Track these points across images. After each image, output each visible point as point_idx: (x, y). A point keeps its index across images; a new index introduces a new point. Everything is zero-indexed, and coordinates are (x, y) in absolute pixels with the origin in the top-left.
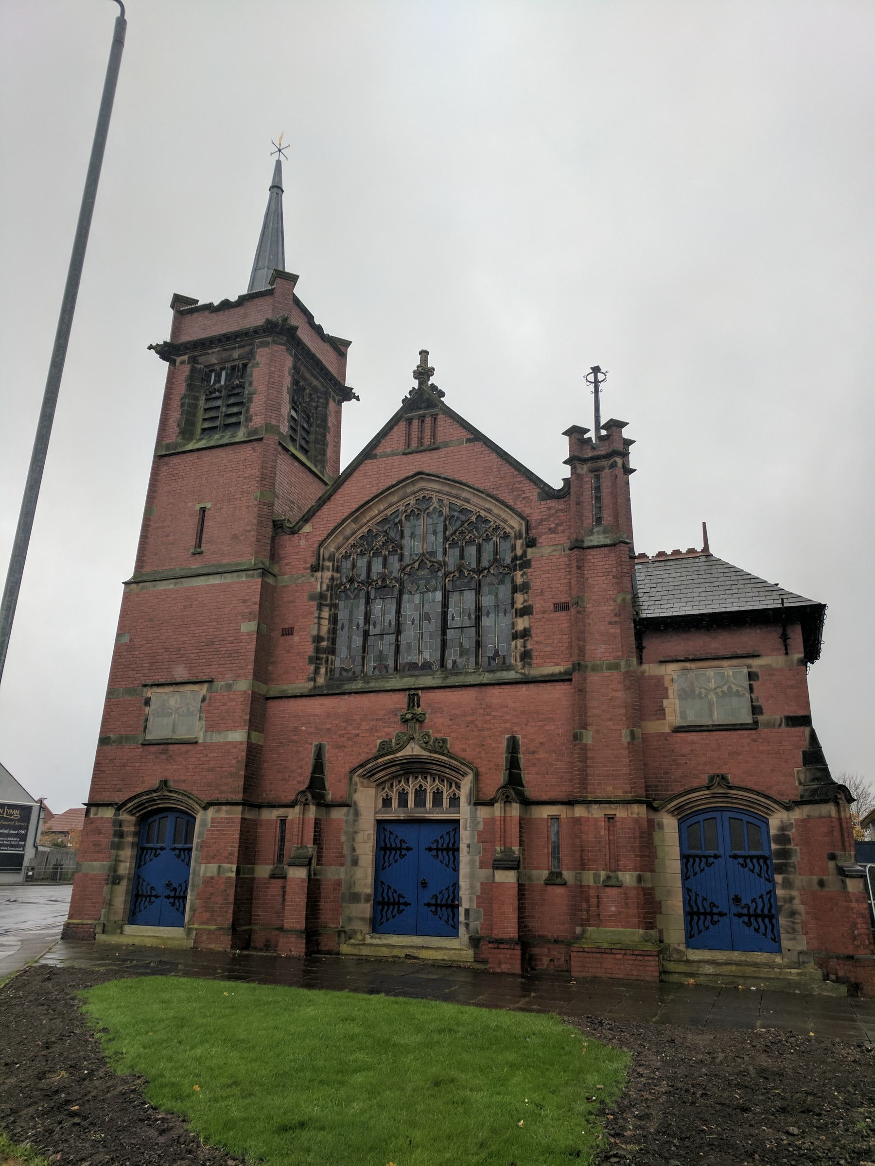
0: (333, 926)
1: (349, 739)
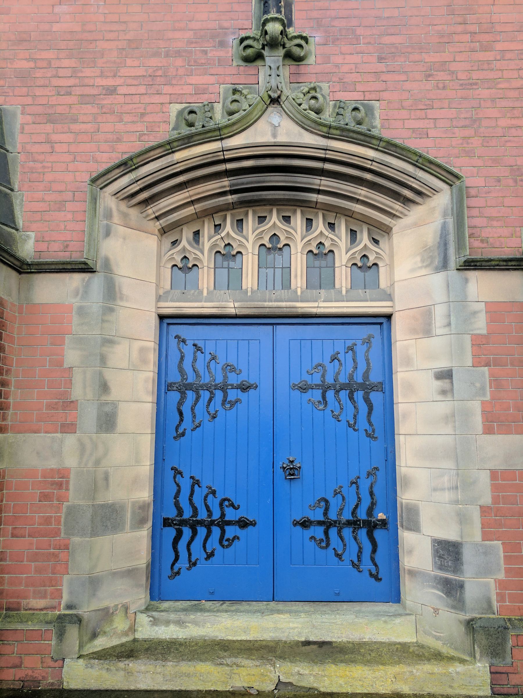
0: (40, 603)
1: (84, 99)
